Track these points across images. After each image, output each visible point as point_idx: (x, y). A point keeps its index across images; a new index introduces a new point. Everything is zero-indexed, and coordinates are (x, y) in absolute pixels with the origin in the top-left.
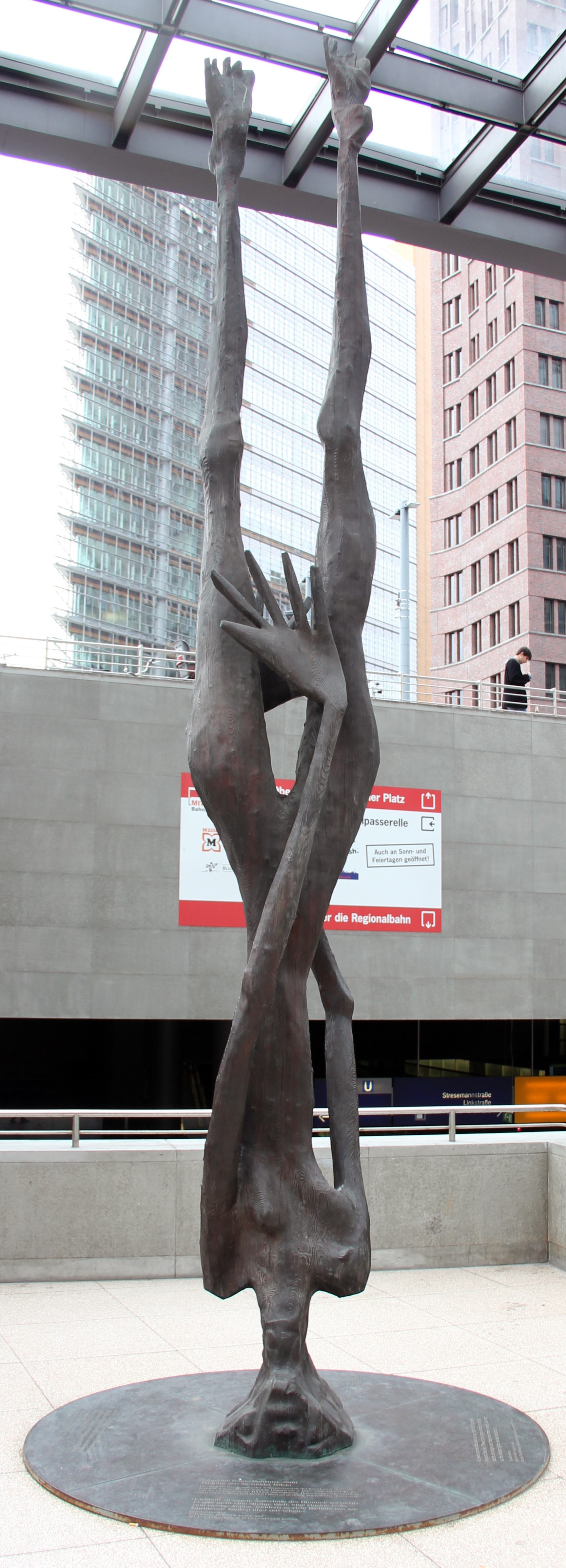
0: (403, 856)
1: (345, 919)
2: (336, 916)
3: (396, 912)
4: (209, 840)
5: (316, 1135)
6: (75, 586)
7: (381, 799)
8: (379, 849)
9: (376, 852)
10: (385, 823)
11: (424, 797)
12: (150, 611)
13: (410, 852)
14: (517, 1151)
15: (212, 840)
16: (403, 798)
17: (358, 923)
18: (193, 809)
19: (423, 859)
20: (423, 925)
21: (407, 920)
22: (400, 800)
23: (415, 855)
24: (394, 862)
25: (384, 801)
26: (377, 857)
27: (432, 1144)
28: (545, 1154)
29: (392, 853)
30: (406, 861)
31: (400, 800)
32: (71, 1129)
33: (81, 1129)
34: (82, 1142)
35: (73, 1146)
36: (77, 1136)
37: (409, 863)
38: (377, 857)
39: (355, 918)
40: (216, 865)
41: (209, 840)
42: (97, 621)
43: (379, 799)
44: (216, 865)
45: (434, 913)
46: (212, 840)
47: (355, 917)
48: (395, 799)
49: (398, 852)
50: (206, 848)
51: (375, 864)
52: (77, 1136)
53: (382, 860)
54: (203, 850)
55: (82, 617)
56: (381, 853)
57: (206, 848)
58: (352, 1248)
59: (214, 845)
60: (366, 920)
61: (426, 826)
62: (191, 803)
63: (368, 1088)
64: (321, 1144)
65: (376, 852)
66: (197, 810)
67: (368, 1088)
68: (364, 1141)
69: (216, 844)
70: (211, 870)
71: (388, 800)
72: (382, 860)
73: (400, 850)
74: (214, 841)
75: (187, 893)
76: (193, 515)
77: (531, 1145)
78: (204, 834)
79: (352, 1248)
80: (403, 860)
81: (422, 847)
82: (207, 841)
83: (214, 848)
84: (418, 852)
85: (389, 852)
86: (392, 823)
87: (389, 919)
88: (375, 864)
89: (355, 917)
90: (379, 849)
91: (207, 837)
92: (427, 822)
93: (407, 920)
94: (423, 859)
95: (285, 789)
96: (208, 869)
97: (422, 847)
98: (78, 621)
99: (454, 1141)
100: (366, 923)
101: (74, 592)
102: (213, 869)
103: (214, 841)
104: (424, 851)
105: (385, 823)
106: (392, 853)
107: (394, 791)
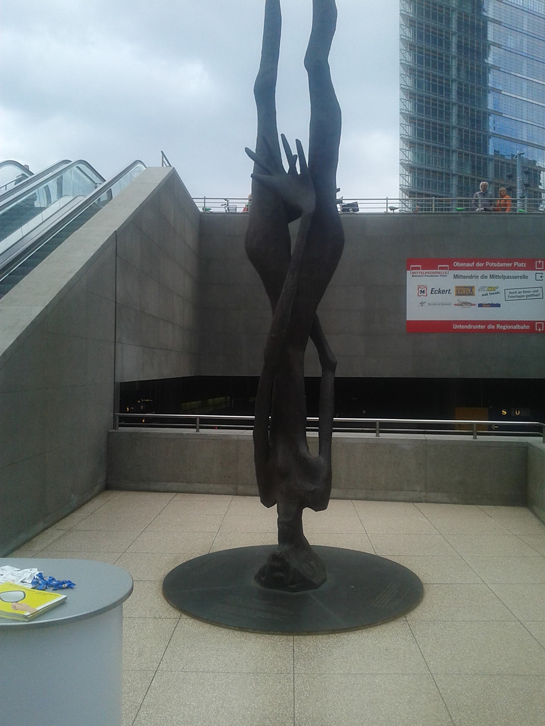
0: (525, 294)
1: (493, 327)
2: (488, 326)
3: (521, 323)
4: (421, 291)
5: (308, 430)
6: (411, 173)
7: (513, 265)
8: (512, 291)
9: (510, 293)
10: (516, 277)
11: (537, 263)
12: (449, 182)
13: (530, 292)
14: (509, 445)
15: (422, 291)
16: (525, 264)
17: (500, 329)
18: (413, 276)
19: (536, 295)
20: (536, 330)
21: (528, 327)
22: (523, 265)
23: (532, 293)
24: (520, 297)
25: (487, 266)
26: (511, 295)
27: (464, 439)
28: (526, 449)
29: (519, 293)
30: (527, 297)
31: (523, 265)
32: (375, 428)
33: (200, 424)
34: (200, 430)
35: (197, 432)
36: (198, 427)
37: (529, 298)
38: (511, 295)
39: (499, 327)
40: (425, 302)
41: (421, 291)
42: (423, 189)
43: (484, 265)
44: (425, 302)
45: (543, 323)
46: (422, 291)
47: (498, 326)
48: (521, 265)
49: (522, 292)
50: (420, 294)
51: (510, 299)
52: (198, 427)
53: (513, 297)
54: (418, 296)
55: (415, 188)
56: (513, 293)
57: (420, 294)
58: (317, 487)
59: (424, 293)
60: (504, 328)
61: (538, 278)
62: (412, 273)
63: (518, 413)
64: (312, 435)
65: (510, 293)
66: (415, 276)
67: (518, 413)
68: (335, 435)
69: (425, 292)
70: (422, 306)
71: (488, 265)
72: (513, 297)
73: (523, 291)
74: (424, 291)
75: (410, 317)
76: (469, 130)
77: (517, 443)
78: (418, 288)
79: (317, 487)
80: (525, 296)
81: (536, 289)
82: (420, 291)
83: (424, 294)
84: (534, 292)
85: (517, 293)
86: (519, 277)
87: (517, 327)
88: (510, 299)
89: (498, 326)
90: (512, 291)
91: (420, 289)
92: (538, 276)
93: (528, 327)
94: (536, 295)
95: (461, 263)
96: (421, 305)
97: (536, 289)
98: (413, 190)
99: (199, 432)
100: (504, 329)
101: (411, 176)
102: (423, 305)
103: (424, 291)
104: (537, 291)
105: (516, 277)
106: (519, 293)
107: (520, 261)
